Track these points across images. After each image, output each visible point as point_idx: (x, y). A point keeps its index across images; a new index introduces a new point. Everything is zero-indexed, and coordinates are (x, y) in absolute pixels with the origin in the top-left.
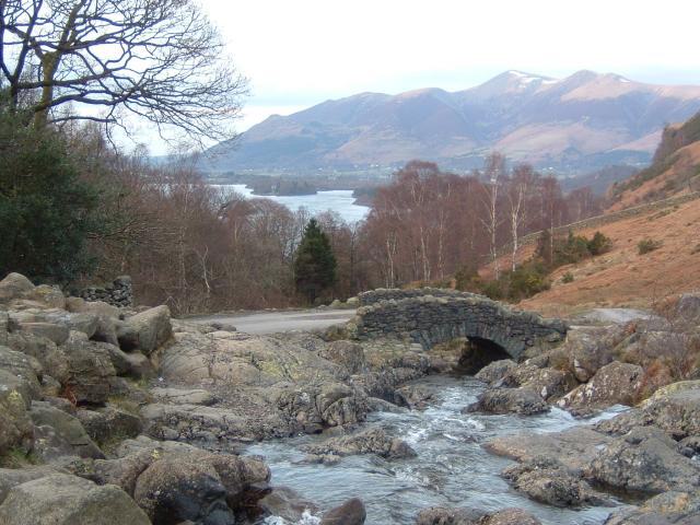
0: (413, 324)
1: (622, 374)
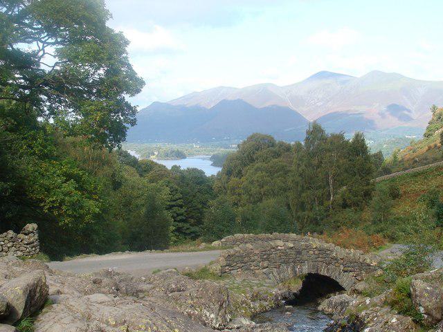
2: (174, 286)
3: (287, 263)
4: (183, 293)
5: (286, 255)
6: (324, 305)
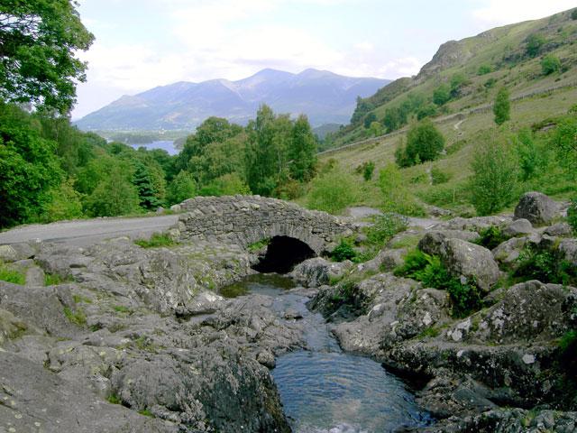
0: (230, 227)
1: (550, 298)
2: (119, 258)
5: (254, 217)
6: (297, 272)
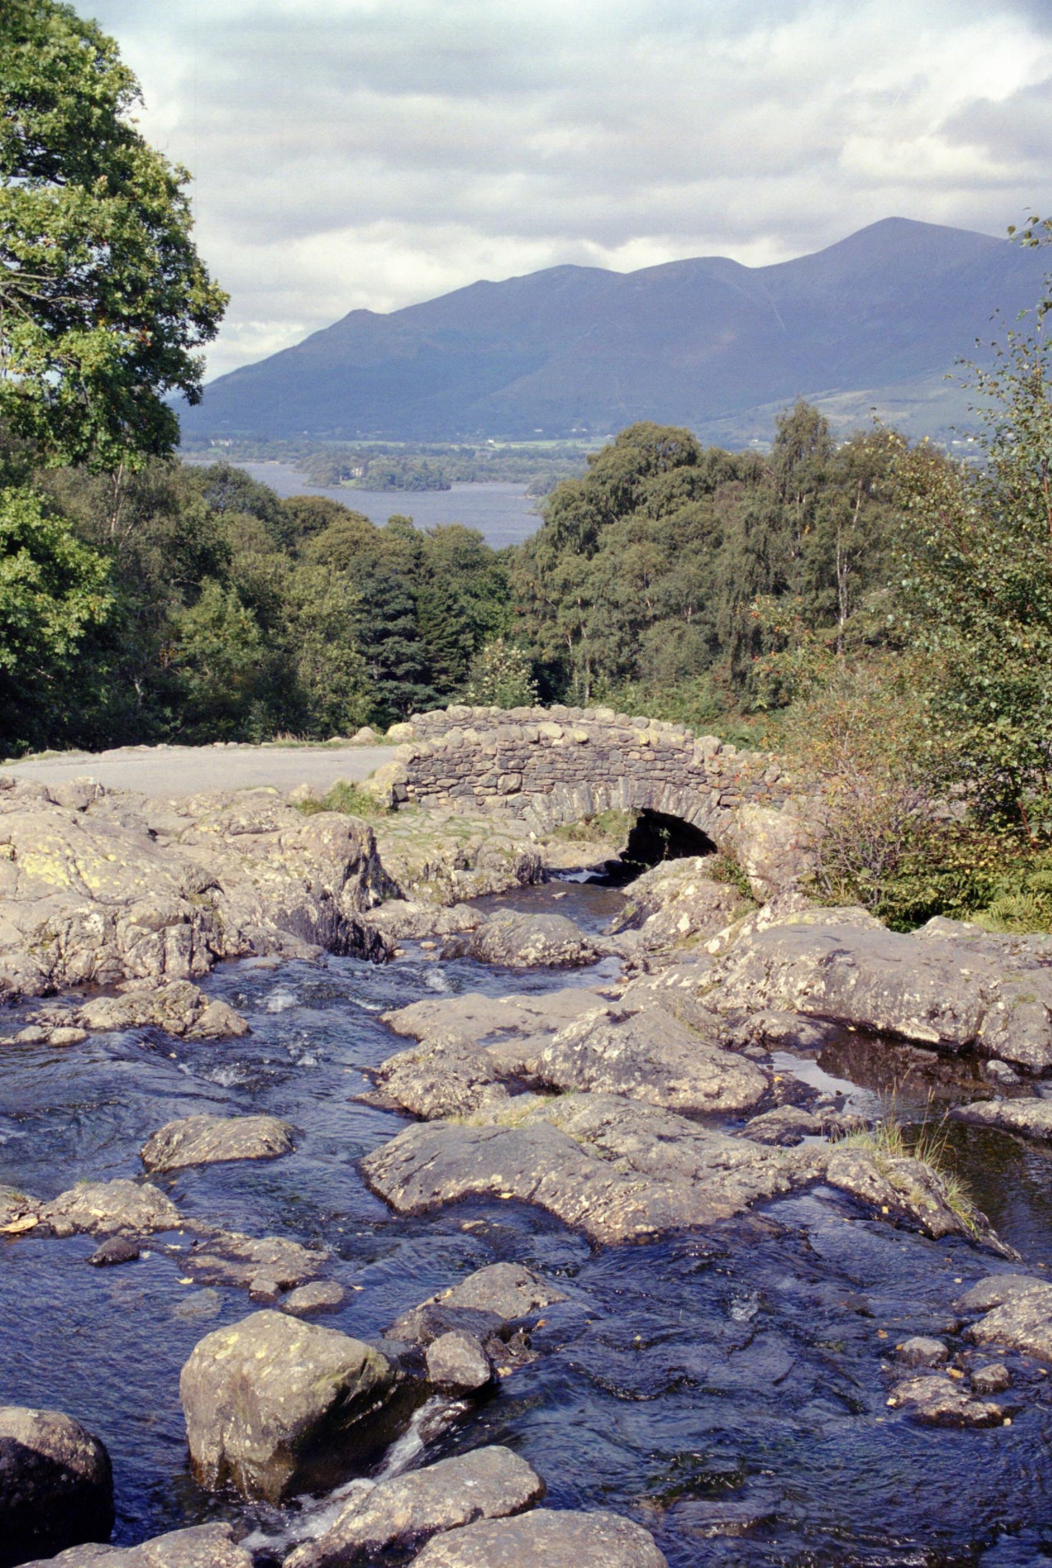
2: (244, 822)
3: (569, 780)
4: (263, 838)
